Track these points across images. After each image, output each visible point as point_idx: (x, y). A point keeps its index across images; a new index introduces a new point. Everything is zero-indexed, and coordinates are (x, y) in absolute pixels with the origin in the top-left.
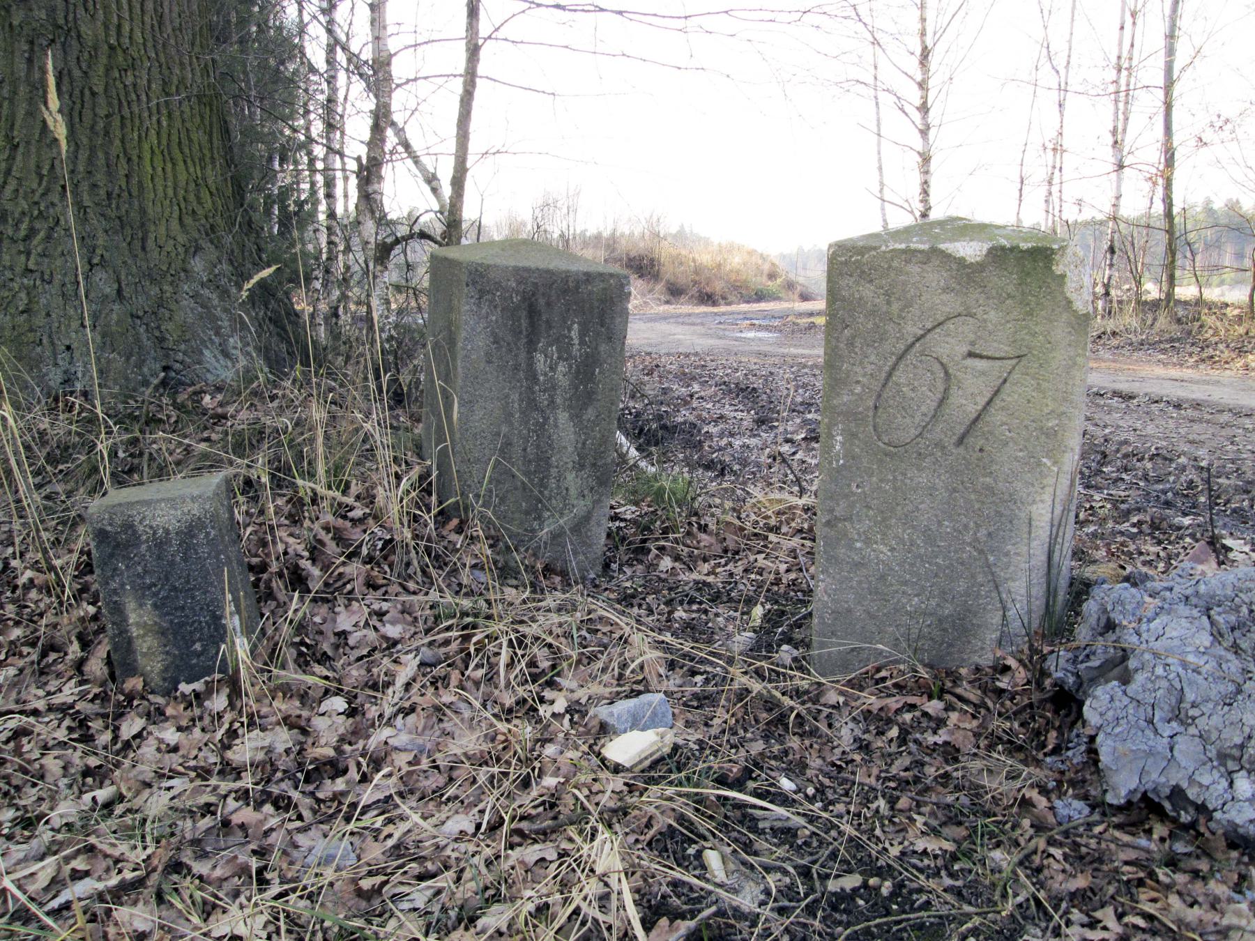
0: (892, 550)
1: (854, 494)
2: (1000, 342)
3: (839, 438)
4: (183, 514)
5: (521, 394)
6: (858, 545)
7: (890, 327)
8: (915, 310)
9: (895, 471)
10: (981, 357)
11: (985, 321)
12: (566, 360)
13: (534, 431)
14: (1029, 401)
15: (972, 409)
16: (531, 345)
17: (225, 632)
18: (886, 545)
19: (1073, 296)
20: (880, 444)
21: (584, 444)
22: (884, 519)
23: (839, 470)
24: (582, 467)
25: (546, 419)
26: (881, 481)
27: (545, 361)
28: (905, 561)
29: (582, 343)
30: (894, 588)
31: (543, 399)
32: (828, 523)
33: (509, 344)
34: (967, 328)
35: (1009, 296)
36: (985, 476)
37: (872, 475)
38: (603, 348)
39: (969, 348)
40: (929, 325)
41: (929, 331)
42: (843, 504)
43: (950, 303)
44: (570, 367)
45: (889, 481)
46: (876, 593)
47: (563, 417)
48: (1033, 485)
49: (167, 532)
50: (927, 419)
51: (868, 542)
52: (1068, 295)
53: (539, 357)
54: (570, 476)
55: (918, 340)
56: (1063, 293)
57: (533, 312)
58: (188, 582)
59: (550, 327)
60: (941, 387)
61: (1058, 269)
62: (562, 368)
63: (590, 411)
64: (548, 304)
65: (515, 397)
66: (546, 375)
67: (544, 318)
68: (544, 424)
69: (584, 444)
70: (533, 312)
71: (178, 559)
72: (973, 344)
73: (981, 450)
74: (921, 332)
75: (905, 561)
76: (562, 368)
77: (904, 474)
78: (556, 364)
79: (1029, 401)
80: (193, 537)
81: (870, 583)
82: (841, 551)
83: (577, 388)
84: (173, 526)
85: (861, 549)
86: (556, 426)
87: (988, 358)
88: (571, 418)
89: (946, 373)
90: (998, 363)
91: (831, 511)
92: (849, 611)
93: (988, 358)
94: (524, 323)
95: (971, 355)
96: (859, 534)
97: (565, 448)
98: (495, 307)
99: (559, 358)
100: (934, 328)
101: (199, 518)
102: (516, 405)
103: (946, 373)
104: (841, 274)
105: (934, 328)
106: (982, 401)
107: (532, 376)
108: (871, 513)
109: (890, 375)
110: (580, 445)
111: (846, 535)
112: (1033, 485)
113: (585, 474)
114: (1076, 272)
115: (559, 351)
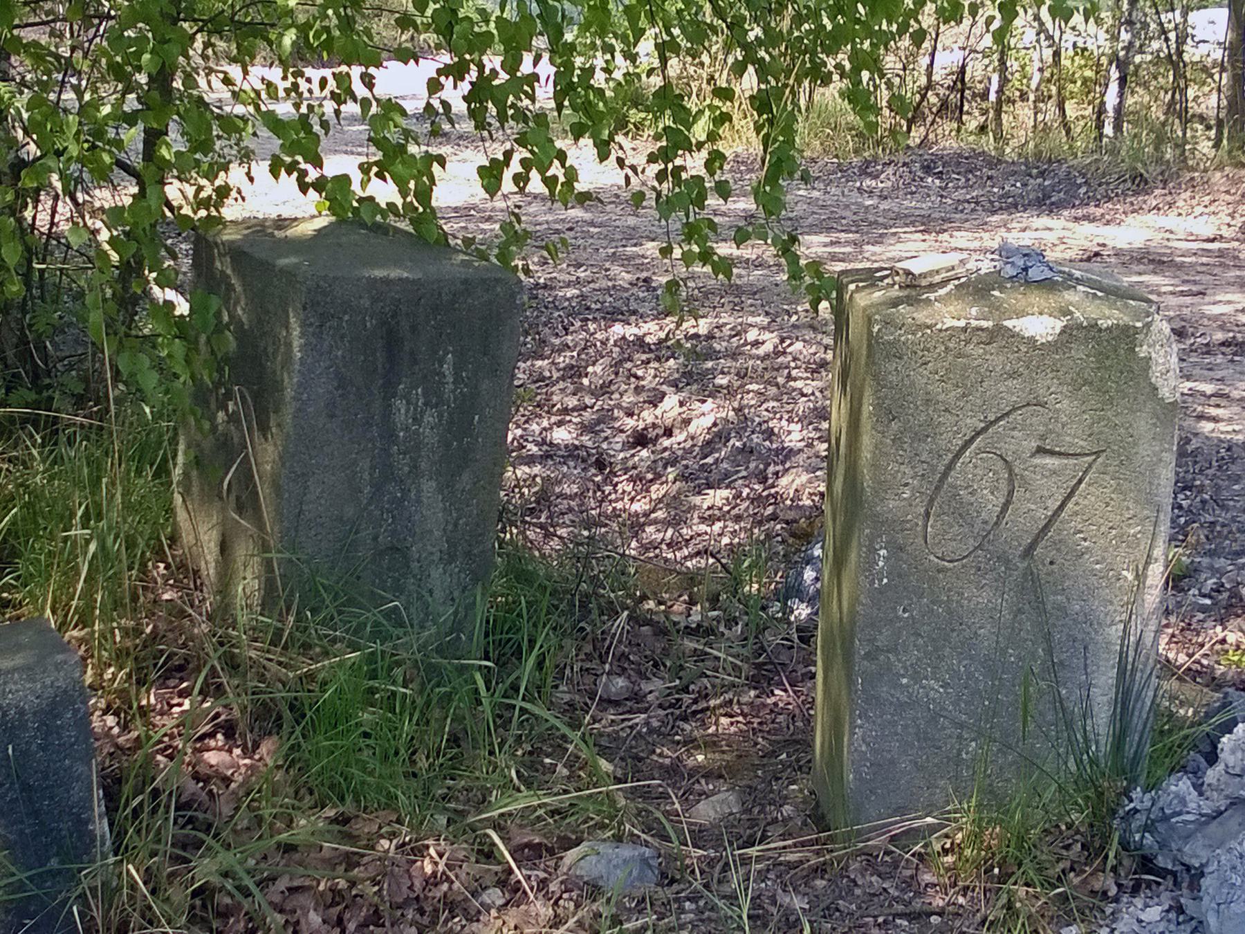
0: (945, 685)
1: (899, 619)
2: (1075, 436)
3: (883, 552)
4: (44, 686)
5: (373, 458)
6: (905, 681)
7: (947, 419)
8: (975, 399)
9: (950, 590)
10: (1052, 453)
11: (1058, 411)
12: (436, 406)
13: (388, 511)
14: (1107, 505)
15: (1042, 515)
16: (389, 390)
17: (93, 840)
18: (937, 680)
19: (1159, 383)
20: (932, 557)
21: (456, 525)
22: (936, 649)
23: (882, 590)
24: (452, 558)
25: (405, 492)
26: (933, 602)
27: (407, 411)
28: (960, 699)
29: (457, 377)
30: (948, 732)
31: (403, 465)
32: (868, 656)
33: (358, 389)
34: (1037, 422)
35: (1086, 382)
36: (1055, 593)
37: (922, 596)
38: (485, 385)
39: (1039, 443)
40: (992, 417)
41: (992, 423)
42: (886, 632)
43: (1011, 393)
44: (440, 416)
45: (942, 602)
46: (925, 740)
47: (429, 486)
48: (1111, 603)
49: (22, 712)
50: (989, 528)
51: (916, 678)
52: (1153, 380)
53: (400, 404)
54: (436, 573)
55: (978, 434)
56: (1147, 378)
57: (392, 342)
58: (46, 778)
59: (415, 362)
60: (1004, 486)
61: (1142, 352)
62: (429, 418)
63: (466, 476)
64: (414, 329)
65: (365, 464)
66: (407, 429)
67: (407, 348)
68: (403, 499)
69: (456, 525)
70: (392, 342)
71: (34, 747)
72: (1043, 437)
73: (1052, 563)
74: (983, 425)
75: (960, 699)
76: (429, 418)
77: (961, 594)
78: (422, 413)
79: (1107, 505)
80: (57, 717)
81: (918, 726)
82: (884, 690)
83: (448, 446)
84: (30, 702)
85: (907, 686)
86: (419, 501)
87: (1060, 454)
88: (440, 490)
89: (1011, 472)
90: (1072, 461)
91: (872, 641)
92: (892, 762)
93: (1060, 454)
94: (380, 357)
95: (1041, 451)
96: (905, 668)
97: (431, 531)
98: (342, 337)
99: (425, 404)
100: (998, 419)
101: (65, 692)
102: (366, 476)
103: (1011, 472)
104: (887, 356)
105: (998, 419)
106: (1053, 505)
107: (390, 435)
108: (920, 641)
109: (945, 475)
110: (450, 527)
111: (889, 669)
112: (1111, 603)
113: (454, 568)
114: (1162, 353)
115: (425, 394)
